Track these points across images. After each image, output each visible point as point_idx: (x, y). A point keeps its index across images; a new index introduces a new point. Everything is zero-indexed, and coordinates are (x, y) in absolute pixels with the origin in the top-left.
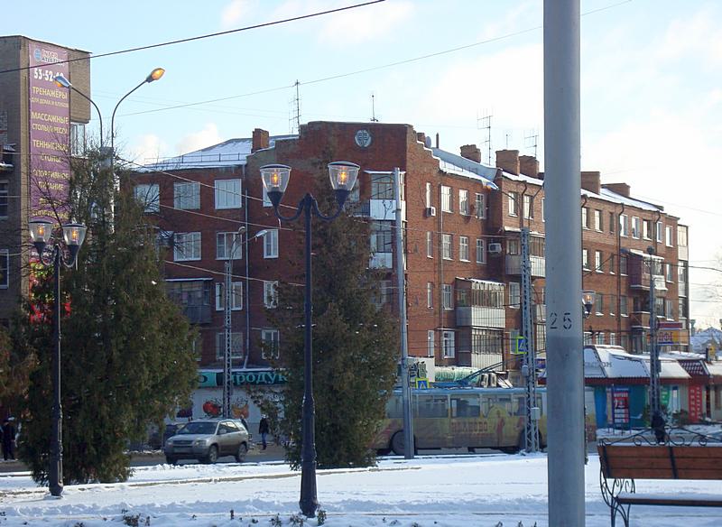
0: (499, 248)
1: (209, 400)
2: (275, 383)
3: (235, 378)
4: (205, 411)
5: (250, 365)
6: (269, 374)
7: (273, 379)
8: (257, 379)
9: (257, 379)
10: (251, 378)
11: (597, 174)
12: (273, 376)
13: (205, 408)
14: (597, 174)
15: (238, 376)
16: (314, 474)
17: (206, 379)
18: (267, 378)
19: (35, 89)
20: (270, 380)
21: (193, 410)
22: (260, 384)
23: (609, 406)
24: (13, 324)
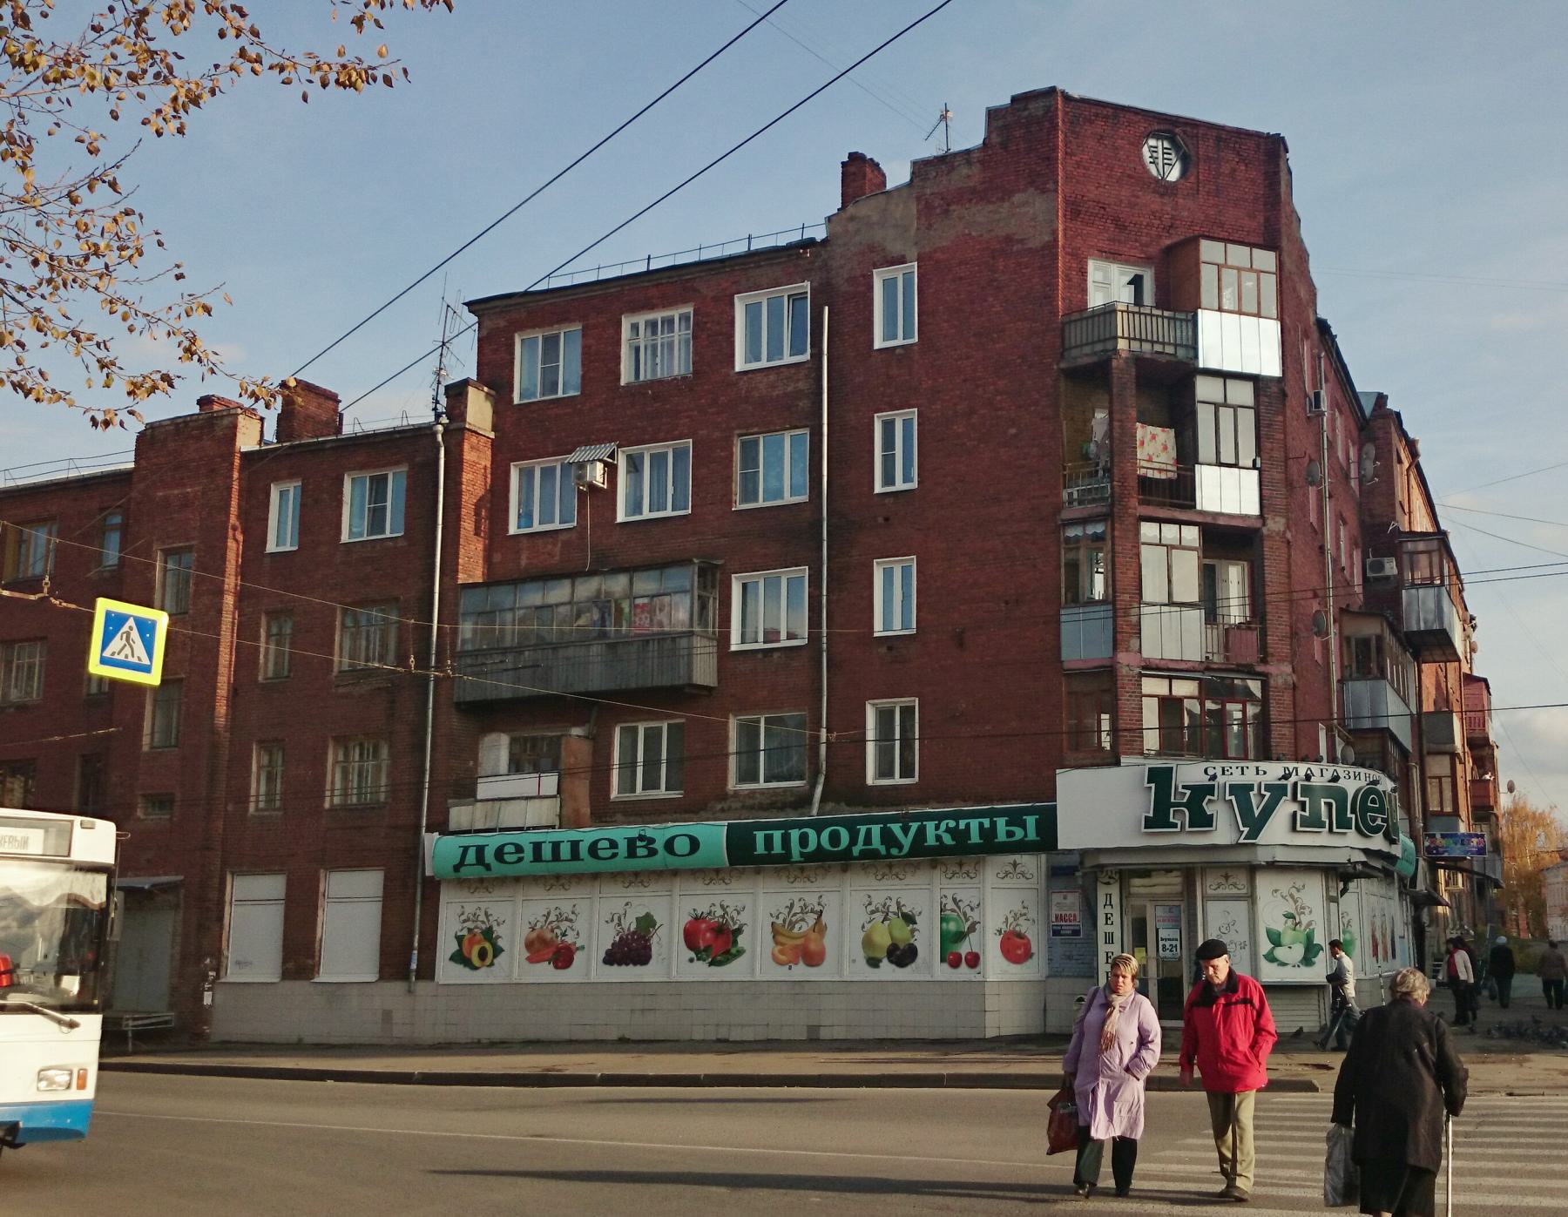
0: (1391, 568)
1: (703, 908)
2: (912, 853)
3: (786, 840)
4: (781, 964)
5: (830, 805)
6: (896, 828)
7: (907, 842)
8: (853, 841)
9: (853, 841)
10: (834, 838)
11: (843, 163)
12: (906, 830)
13: (691, 938)
14: (843, 163)
15: (795, 834)
16: (1136, 544)
17: (694, 844)
18: (888, 838)
19: (655, 684)
20: (900, 847)
21: (654, 941)
22: (865, 854)
23: (1170, 903)
24: (961, 836)
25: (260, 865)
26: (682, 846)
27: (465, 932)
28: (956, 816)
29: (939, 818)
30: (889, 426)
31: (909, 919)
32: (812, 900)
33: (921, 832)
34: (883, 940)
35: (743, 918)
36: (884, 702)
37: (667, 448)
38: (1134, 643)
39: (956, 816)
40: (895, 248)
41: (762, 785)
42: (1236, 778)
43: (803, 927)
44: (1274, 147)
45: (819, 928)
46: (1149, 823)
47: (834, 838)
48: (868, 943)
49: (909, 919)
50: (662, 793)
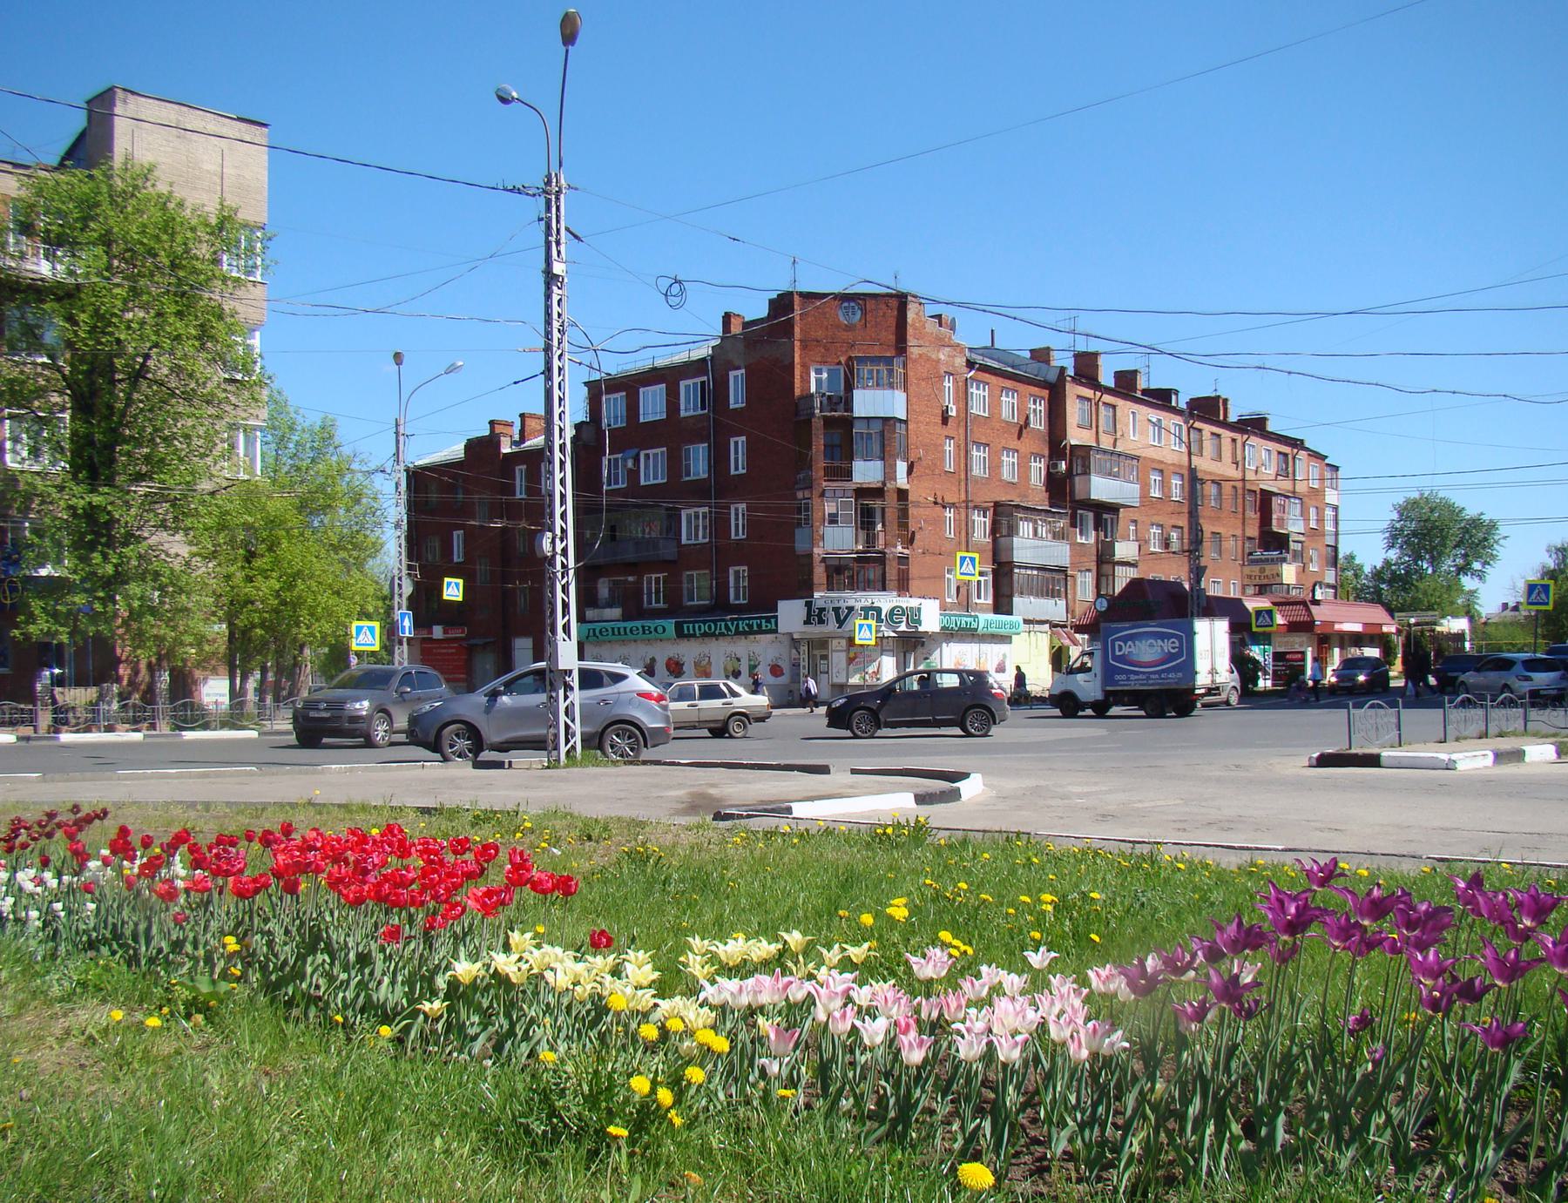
10: (710, 628)
13: (668, 666)
25: (524, 633)
26: (660, 629)
27: (1224, 696)
28: (749, 619)
29: (744, 619)
30: (736, 443)
31: (739, 660)
32: (707, 652)
33: (738, 625)
34: (730, 669)
35: (684, 659)
36: (737, 568)
37: (658, 451)
38: (821, 544)
39: (749, 619)
40: (737, 363)
41: (696, 603)
42: (864, 603)
43: (704, 663)
44: (901, 301)
45: (709, 663)
46: (805, 623)
47: (710, 628)
48: (725, 669)
49: (739, 660)
50: (661, 605)
